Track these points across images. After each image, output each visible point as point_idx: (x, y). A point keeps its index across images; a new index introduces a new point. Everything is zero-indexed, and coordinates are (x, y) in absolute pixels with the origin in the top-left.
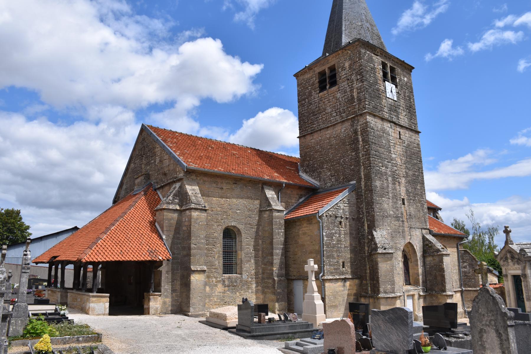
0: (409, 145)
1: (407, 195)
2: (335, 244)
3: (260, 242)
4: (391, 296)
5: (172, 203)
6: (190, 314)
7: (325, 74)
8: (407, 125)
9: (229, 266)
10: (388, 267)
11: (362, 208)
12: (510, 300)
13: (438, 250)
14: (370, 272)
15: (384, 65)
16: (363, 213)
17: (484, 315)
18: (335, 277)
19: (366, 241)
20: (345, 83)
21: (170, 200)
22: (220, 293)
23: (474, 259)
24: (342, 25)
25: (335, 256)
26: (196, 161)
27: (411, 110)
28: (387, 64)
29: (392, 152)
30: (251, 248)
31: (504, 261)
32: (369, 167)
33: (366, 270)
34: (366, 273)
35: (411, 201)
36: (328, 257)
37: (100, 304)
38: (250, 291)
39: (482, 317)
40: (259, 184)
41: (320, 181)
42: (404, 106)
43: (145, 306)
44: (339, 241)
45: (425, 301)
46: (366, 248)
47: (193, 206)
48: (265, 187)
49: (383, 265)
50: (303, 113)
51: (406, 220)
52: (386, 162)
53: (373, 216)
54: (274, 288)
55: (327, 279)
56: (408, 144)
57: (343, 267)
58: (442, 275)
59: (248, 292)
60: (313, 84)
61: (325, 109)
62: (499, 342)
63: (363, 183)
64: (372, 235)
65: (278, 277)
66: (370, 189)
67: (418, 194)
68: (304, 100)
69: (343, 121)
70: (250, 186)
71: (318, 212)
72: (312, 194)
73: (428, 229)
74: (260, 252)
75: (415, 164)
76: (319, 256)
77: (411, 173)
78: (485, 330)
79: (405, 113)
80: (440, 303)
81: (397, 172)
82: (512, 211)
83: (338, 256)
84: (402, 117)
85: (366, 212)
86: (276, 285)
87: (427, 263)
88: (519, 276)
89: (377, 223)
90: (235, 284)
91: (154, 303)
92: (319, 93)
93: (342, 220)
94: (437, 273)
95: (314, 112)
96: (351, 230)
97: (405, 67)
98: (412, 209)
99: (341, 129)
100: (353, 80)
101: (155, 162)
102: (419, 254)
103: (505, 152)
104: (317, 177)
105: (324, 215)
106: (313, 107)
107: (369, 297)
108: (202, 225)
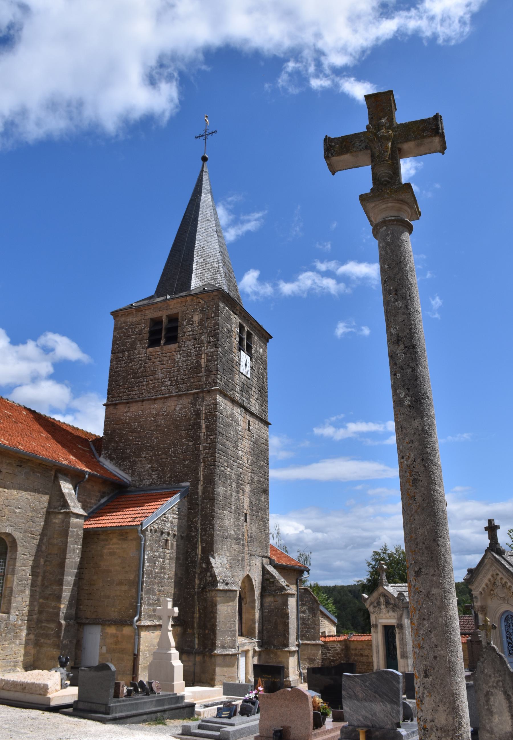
0: (257, 440)
1: (250, 509)
2: (158, 573)
3: (42, 561)
4: (231, 653)
7: (161, 322)
8: (256, 412)
10: (229, 610)
11: (196, 522)
12: (378, 657)
13: (282, 588)
14: (200, 617)
15: (241, 328)
16: (197, 530)
17: (490, 676)
18: (153, 623)
19: (198, 571)
20: (191, 343)
23: (316, 601)
24: (193, 261)
25: (156, 591)
27: (263, 391)
29: (239, 448)
30: (28, 571)
31: (375, 607)
32: (212, 465)
33: (194, 613)
34: (193, 618)
38: (18, 642)
39: (488, 678)
40: (51, 470)
41: (132, 474)
42: (256, 387)
44: (163, 568)
45: (259, 660)
46: (197, 581)
48: (60, 476)
49: (223, 607)
50: (118, 371)
51: (246, 544)
54: (59, 637)
55: (144, 626)
56: (256, 438)
58: (285, 622)
59: (15, 644)
60: (140, 333)
61: (154, 373)
62: (507, 705)
63: (200, 488)
64: (209, 563)
65: (65, 619)
66: (210, 497)
67: (261, 508)
68: (123, 352)
69: (180, 396)
70: (39, 472)
71: (141, 524)
72: (118, 495)
73: (269, 558)
74: (40, 579)
75: (261, 467)
76: (134, 590)
77: (256, 478)
78: (492, 692)
79: (256, 397)
80: (279, 662)
81: (242, 476)
82: (306, 528)
84: (253, 402)
85: (202, 529)
86: (63, 632)
87: (266, 605)
88: (394, 626)
89: (216, 546)
92: (149, 347)
93: (169, 538)
94: (278, 621)
95: (136, 373)
96: (177, 553)
97: (263, 335)
98: (254, 528)
99: (175, 406)
100: (202, 341)
102: (257, 592)
103: (307, 444)
104: (129, 469)
105: (149, 528)
106: (135, 365)
107: (195, 653)
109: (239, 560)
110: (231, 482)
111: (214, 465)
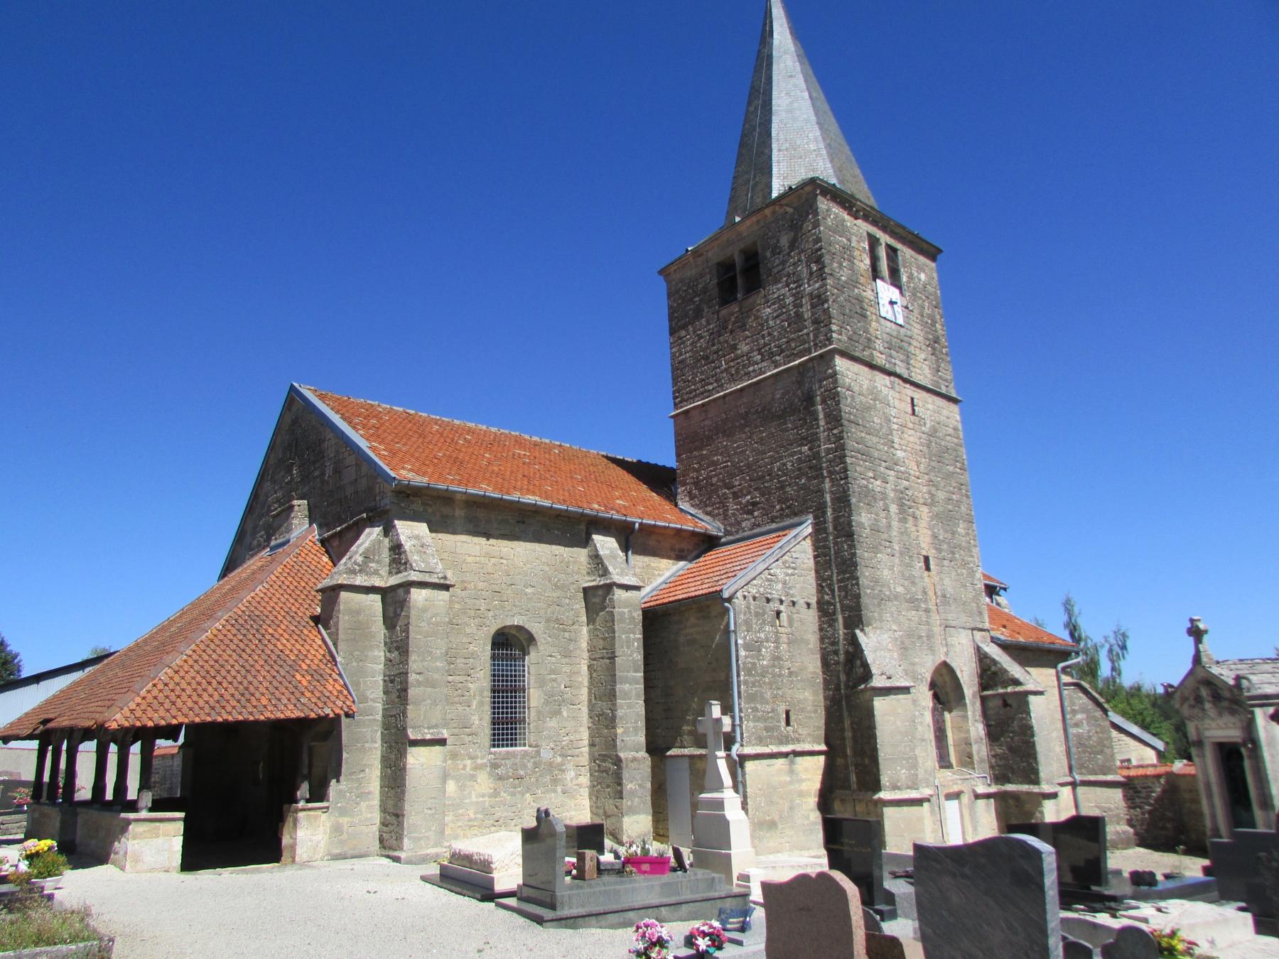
0: (933, 433)
2: (768, 666)
5: (360, 571)
6: (403, 855)
9: (506, 726)
10: (899, 723)
16: (833, 591)
21: (355, 563)
22: (483, 796)
25: (768, 695)
26: (424, 468)
28: (878, 240)
29: (896, 446)
32: (842, 475)
33: (843, 730)
34: (843, 739)
35: (946, 563)
36: (752, 698)
37: (155, 842)
42: (921, 339)
43: (286, 840)
47: (414, 576)
51: (934, 608)
52: (882, 469)
53: (858, 596)
57: (788, 723)
59: (555, 791)
60: (705, 290)
67: (960, 546)
77: (941, 495)
79: (923, 356)
83: (775, 697)
90: (522, 773)
91: (308, 832)
93: (782, 608)
98: (947, 582)
101: (323, 474)
108: (437, 624)
109: (920, 637)
110: (885, 504)
111: (846, 478)
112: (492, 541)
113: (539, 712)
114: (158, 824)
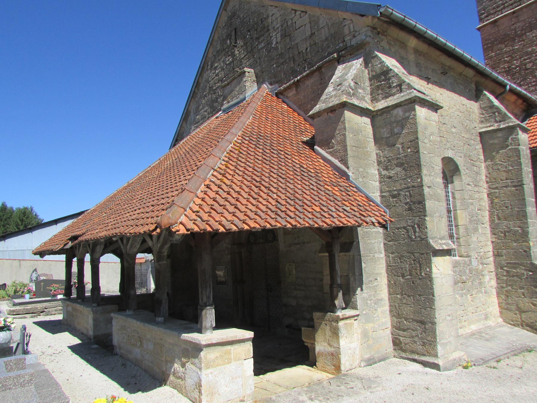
6: (440, 362)
112: (430, 86)
113: (467, 229)
114: (229, 347)
